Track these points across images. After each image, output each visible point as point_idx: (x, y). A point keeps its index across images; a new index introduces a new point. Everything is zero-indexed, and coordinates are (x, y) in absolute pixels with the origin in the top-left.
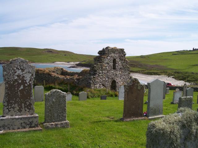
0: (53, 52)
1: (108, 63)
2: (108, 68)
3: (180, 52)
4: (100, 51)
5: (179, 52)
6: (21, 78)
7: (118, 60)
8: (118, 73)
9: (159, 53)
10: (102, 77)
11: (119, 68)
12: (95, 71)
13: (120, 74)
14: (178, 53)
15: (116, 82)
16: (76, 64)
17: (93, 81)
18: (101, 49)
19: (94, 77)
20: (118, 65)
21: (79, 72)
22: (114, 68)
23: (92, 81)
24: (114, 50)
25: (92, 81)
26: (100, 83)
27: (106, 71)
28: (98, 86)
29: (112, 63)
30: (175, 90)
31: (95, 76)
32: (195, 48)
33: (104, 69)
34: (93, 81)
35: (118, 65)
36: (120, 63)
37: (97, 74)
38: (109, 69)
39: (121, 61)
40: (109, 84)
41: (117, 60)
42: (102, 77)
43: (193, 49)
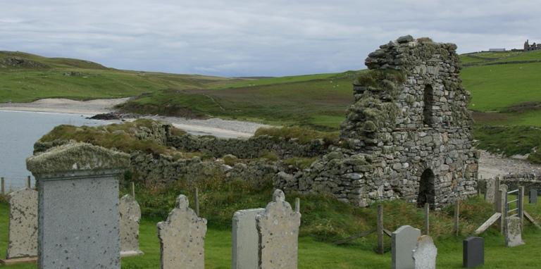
0: (93, 85)
1: (410, 104)
2: (409, 121)
3: (480, 56)
4: (372, 56)
5: (478, 58)
6: (109, 161)
7: (438, 88)
8: (440, 138)
9: (305, 76)
10: (391, 156)
11: (441, 119)
12: (369, 134)
13: (444, 144)
14: (476, 61)
15: (433, 176)
16: (118, 107)
17: (367, 174)
18: (374, 48)
19: (369, 161)
20: (438, 108)
21: (246, 139)
22: (428, 120)
23: (361, 176)
24: (426, 49)
25: (361, 176)
26: (386, 184)
27: (405, 135)
28: (381, 194)
29: (422, 102)
30: (525, 195)
31: (369, 156)
32: (531, 43)
33: (398, 126)
34: (367, 174)
35: (438, 108)
36: (443, 99)
37: (376, 145)
38: (413, 126)
39: (447, 93)
40: (411, 186)
41: (434, 88)
42: (391, 156)
43: (526, 45)
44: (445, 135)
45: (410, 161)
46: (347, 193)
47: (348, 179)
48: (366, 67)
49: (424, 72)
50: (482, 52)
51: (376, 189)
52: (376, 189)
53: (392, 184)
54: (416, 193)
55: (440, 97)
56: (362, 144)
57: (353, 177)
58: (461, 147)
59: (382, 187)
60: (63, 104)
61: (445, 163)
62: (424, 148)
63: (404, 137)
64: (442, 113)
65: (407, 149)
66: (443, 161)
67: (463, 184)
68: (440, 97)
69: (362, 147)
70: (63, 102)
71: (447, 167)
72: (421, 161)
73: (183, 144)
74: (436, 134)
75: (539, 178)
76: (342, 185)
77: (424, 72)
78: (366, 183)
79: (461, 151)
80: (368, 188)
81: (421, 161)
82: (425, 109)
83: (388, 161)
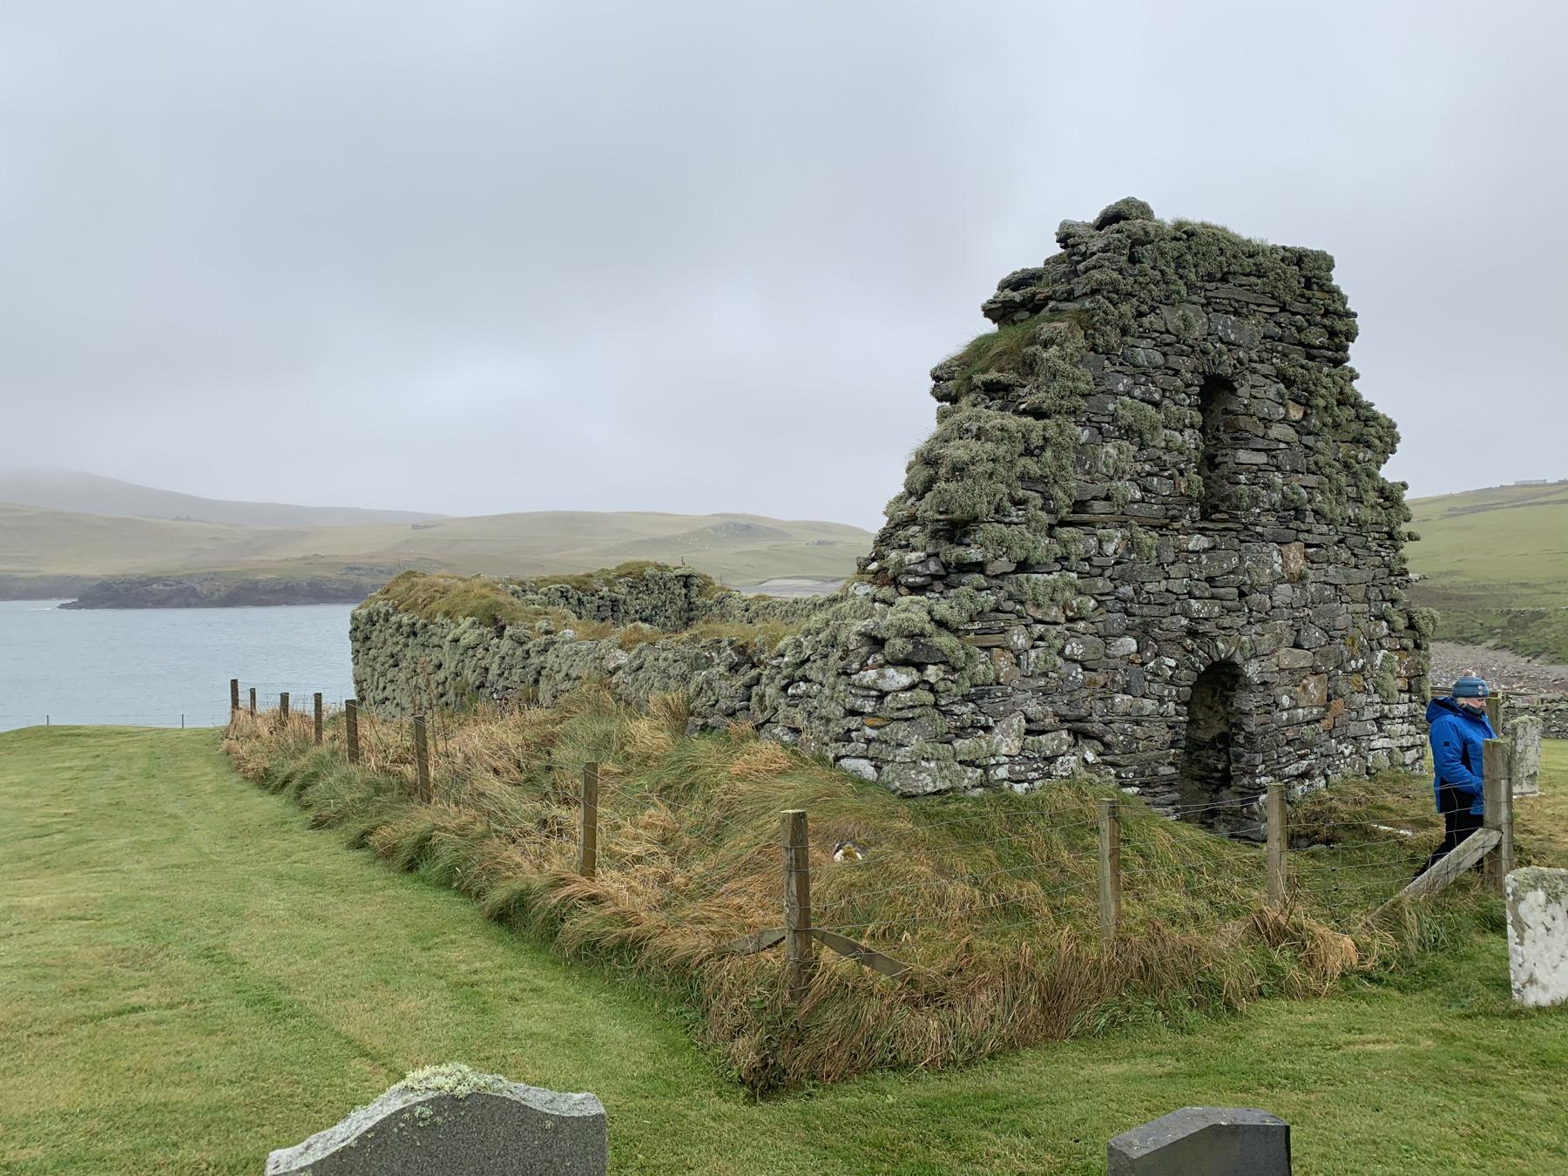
26: (1033, 708)
39: (1296, 413)
41: (1243, 391)
44: (1295, 551)
45: (1143, 633)
46: (869, 741)
47: (869, 688)
48: (990, 327)
49: (1198, 331)
50: (1501, 486)
51: (987, 729)
52: (987, 729)
53: (1064, 710)
54: (1173, 744)
55: (1267, 422)
56: (933, 567)
57: (885, 685)
58: (1360, 595)
59: (1018, 722)
60: (1562, 749)
61: (1297, 645)
62: (1204, 589)
63: (1109, 548)
64: (1278, 479)
65: (1127, 590)
66: (1289, 637)
67: (1369, 714)
68: (1267, 422)
69: (934, 577)
70: (1559, 746)
71: (1302, 659)
72: (1192, 633)
73: (591, 604)
74: (1255, 547)
75: (940, 1175)
76: (853, 713)
77: (1198, 331)
78: (936, 705)
79: (1358, 607)
80: (949, 723)
81: (1192, 633)
82: (1209, 462)
83: (1039, 629)
